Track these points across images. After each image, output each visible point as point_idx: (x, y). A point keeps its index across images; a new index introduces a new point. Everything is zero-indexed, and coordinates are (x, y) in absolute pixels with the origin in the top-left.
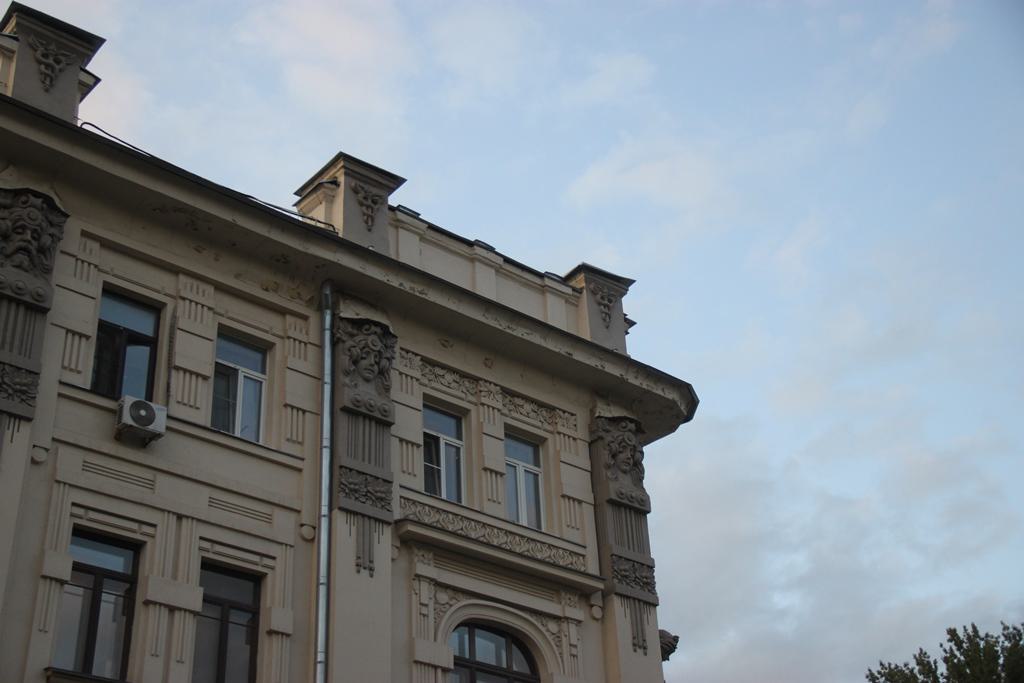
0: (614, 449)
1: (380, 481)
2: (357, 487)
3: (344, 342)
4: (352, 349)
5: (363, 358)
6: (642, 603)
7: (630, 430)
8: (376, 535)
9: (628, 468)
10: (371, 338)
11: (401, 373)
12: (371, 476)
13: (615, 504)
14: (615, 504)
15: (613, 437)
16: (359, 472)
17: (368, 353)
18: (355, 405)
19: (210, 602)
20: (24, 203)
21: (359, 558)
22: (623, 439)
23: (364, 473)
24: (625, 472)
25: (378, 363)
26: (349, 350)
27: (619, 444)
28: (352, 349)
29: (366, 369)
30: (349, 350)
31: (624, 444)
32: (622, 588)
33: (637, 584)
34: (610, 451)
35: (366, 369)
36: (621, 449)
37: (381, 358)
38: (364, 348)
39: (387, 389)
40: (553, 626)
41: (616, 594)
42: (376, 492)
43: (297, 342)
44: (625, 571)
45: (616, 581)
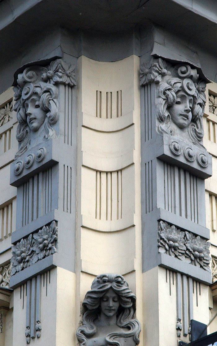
0: (171, 96)
1: (173, 227)
2: (177, 244)
3: (157, 83)
4: (168, 92)
5: (178, 103)
6: (191, 281)
7: (191, 77)
8: (194, 297)
9: (186, 123)
10: (186, 82)
11: (208, 121)
12: (189, 232)
13: (165, 161)
14: (165, 161)
15: (169, 83)
16: (178, 228)
17: (183, 97)
18: (187, 160)
19: (7, 308)
20: (183, 73)
22: (182, 87)
23: (183, 230)
24: (181, 127)
25: (192, 109)
26: (165, 93)
27: (177, 93)
28: (168, 92)
29: (181, 115)
30: (165, 93)
31: (182, 93)
32: (169, 260)
33: (188, 257)
34: (167, 99)
35: (181, 115)
36: (179, 100)
37: (194, 103)
38: (179, 91)
39: (199, 137)
41: (162, 266)
42: (169, 240)
43: (211, 124)
44: (174, 241)
45: (162, 251)
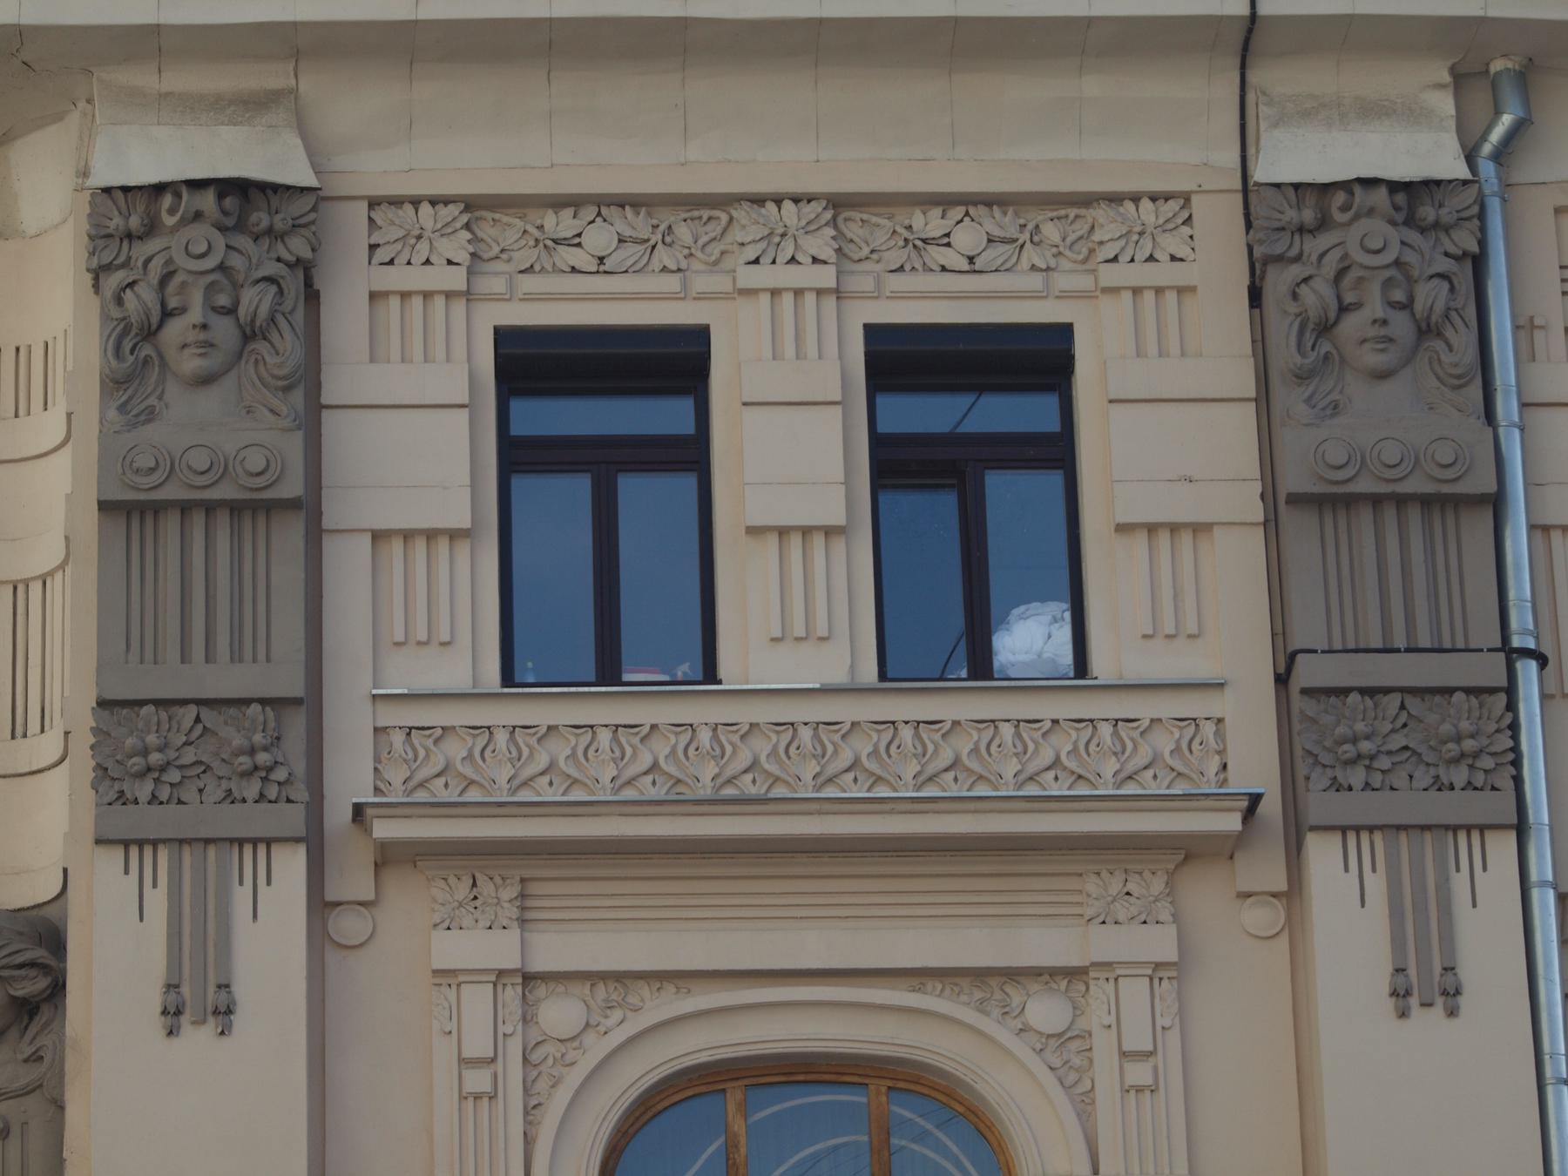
4: (1304, 290)
21: (1399, 971)
40: (1046, 1011)
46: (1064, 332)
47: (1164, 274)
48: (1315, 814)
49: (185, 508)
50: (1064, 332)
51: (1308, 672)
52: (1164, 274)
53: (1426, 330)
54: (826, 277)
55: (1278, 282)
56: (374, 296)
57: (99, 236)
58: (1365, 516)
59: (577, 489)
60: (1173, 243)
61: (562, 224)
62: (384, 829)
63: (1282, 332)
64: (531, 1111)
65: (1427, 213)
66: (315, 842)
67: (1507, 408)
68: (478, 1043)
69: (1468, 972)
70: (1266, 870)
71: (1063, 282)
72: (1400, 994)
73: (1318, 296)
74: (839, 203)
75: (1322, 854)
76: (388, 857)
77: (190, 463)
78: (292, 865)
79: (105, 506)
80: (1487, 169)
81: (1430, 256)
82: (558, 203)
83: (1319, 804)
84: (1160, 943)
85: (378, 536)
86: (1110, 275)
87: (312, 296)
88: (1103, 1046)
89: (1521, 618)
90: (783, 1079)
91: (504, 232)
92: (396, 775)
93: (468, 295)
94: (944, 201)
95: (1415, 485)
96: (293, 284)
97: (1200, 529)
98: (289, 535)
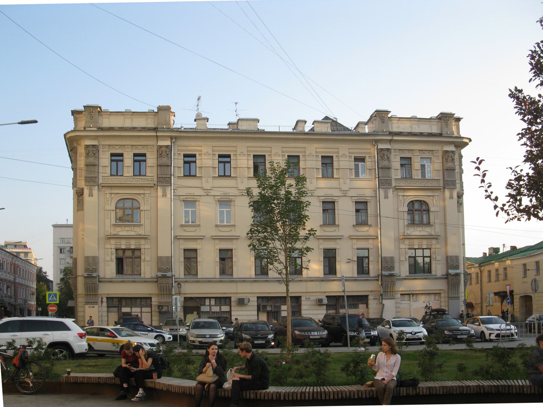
46: (123, 153)
47: (152, 150)
48: (158, 185)
49: (90, 165)
50: (123, 153)
51: (159, 176)
52: (152, 150)
53: (94, 154)
54: (131, 150)
55: (158, 151)
56: (103, 151)
57: (85, 148)
58: (163, 167)
59: (116, 163)
60: (152, 148)
61: (114, 146)
62: (102, 185)
63: (158, 154)
64: (111, 201)
65: (168, 147)
66: (98, 186)
67: (173, 159)
68: (108, 197)
69: (389, 196)
70: (155, 188)
71: (146, 150)
72: (450, 198)
73: (161, 152)
74: (132, 145)
75: (159, 187)
76: (103, 186)
77: (483, 161)
78: (96, 187)
79: (85, 165)
80: (173, 144)
81: (168, 150)
82: (114, 145)
83: (159, 184)
84: (149, 192)
85: (103, 166)
86: (148, 150)
87: (99, 151)
88: (434, 200)
89: (172, 173)
90: (378, 202)
91: (111, 147)
92: (103, 181)
93: (132, 151)
94: (138, 145)
95: (92, 164)
96: (97, 151)
97: (153, 166)
98: (97, 167)
